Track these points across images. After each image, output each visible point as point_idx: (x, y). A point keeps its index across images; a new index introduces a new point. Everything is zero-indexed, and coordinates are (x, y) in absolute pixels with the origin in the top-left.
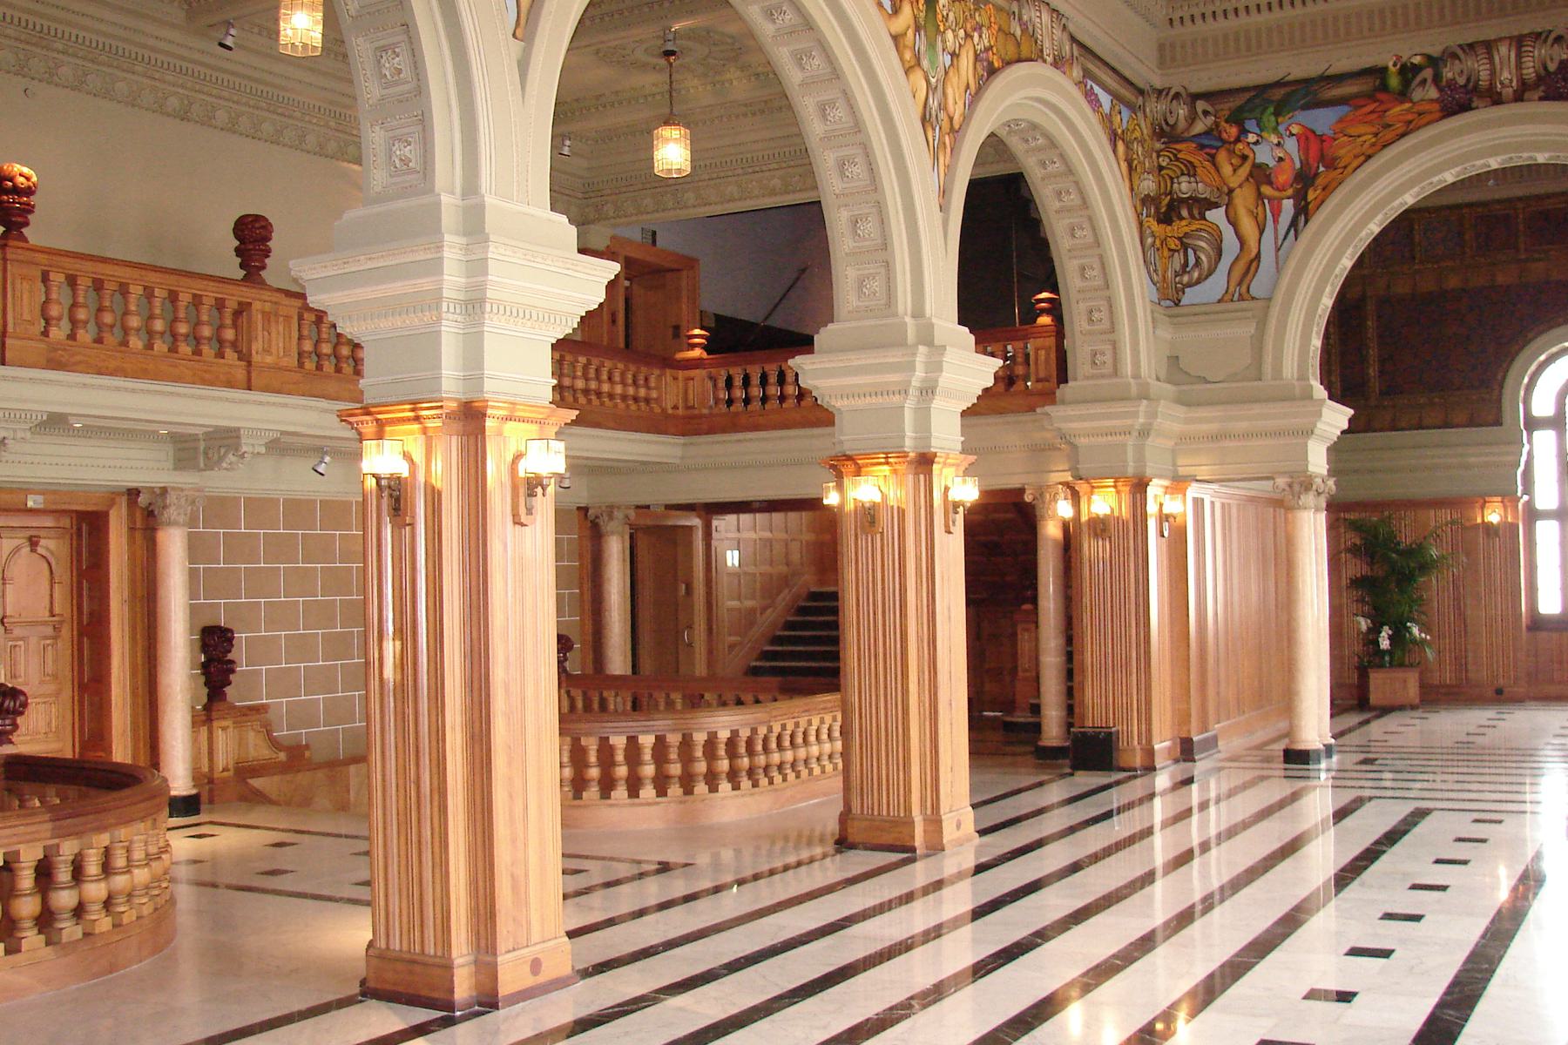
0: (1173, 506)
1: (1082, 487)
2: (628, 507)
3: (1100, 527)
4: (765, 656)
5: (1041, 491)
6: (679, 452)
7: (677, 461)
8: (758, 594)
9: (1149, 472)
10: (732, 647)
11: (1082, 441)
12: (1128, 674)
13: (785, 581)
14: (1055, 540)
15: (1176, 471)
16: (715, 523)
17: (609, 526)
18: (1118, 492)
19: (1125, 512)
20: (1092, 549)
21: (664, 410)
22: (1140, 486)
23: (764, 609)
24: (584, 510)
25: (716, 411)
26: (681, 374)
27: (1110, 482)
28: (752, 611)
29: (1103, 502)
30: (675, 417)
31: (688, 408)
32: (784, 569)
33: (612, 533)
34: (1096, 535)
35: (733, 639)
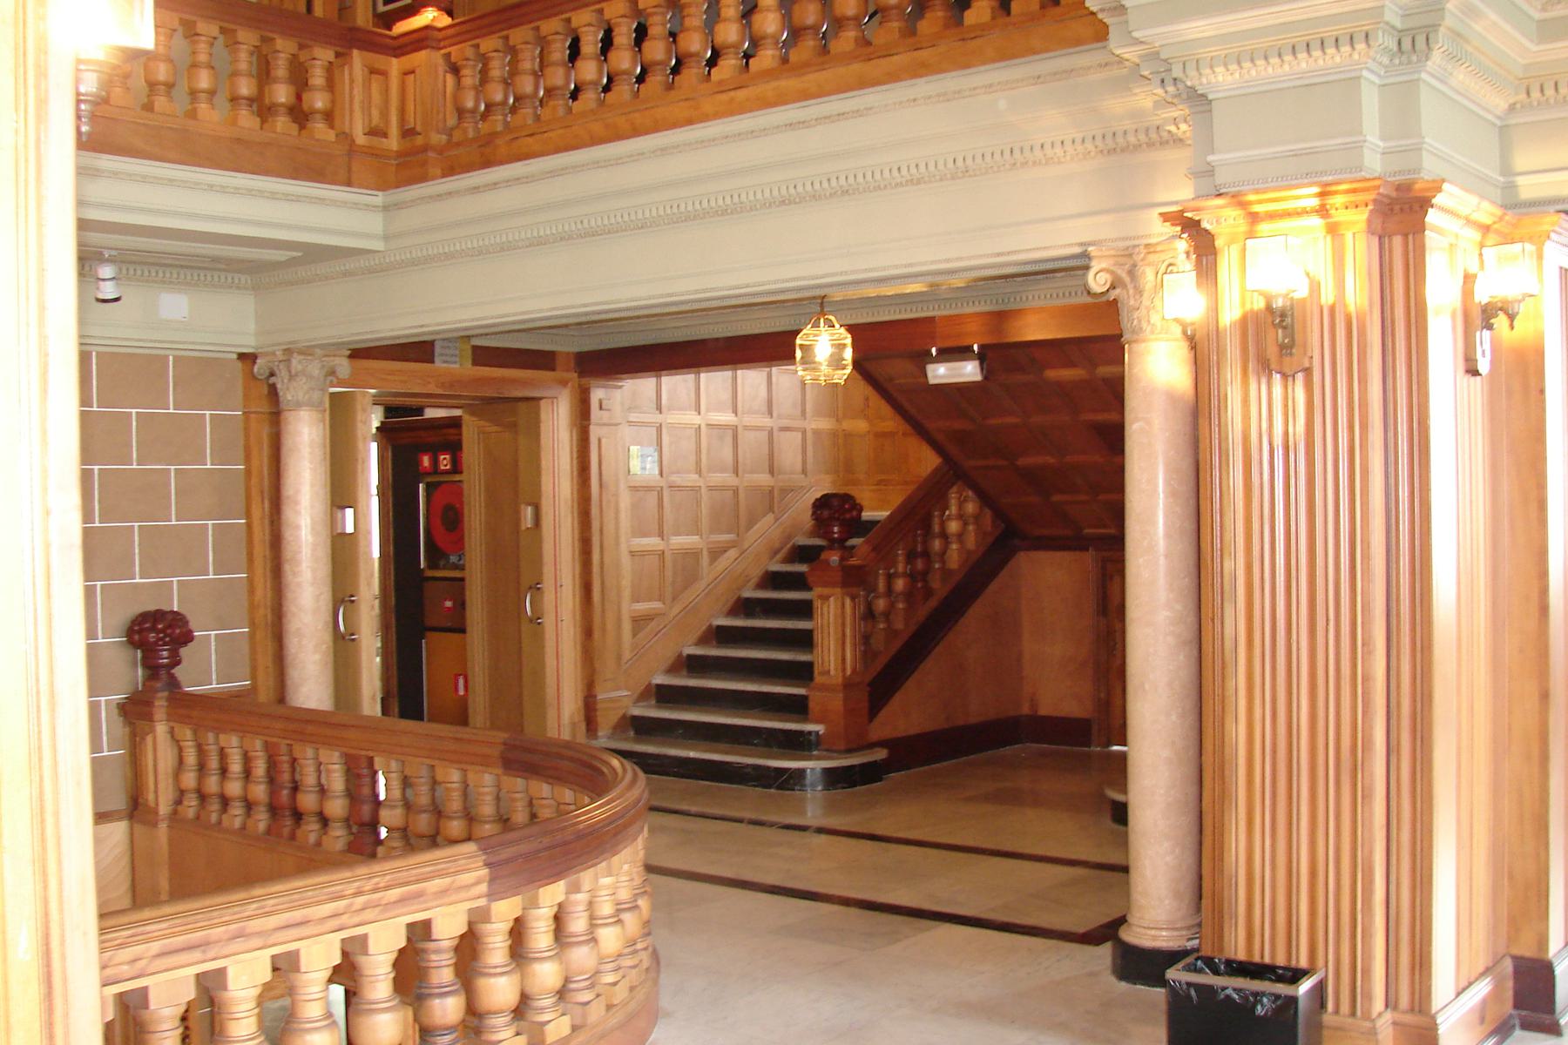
0: (1508, 274)
1: (1222, 220)
2: (331, 349)
3: (1276, 338)
4: (723, 635)
5: (1130, 260)
6: (375, 223)
7: (378, 245)
8: (705, 523)
9: (1430, 168)
10: (639, 621)
11: (1220, 80)
12: (1361, 796)
13: (771, 500)
14: (1172, 397)
15: (1510, 187)
16: (597, 394)
17: (290, 393)
18: (1333, 230)
19: (1358, 295)
20: (1261, 411)
21: (346, 137)
22: (1402, 212)
23: (716, 553)
24: (247, 358)
25: (457, 136)
26: (395, 65)
27: (1307, 197)
28: (692, 555)
29: (1296, 257)
30: (373, 153)
31: (407, 133)
32: (763, 479)
33: (299, 405)
34: (1265, 368)
35: (643, 607)
